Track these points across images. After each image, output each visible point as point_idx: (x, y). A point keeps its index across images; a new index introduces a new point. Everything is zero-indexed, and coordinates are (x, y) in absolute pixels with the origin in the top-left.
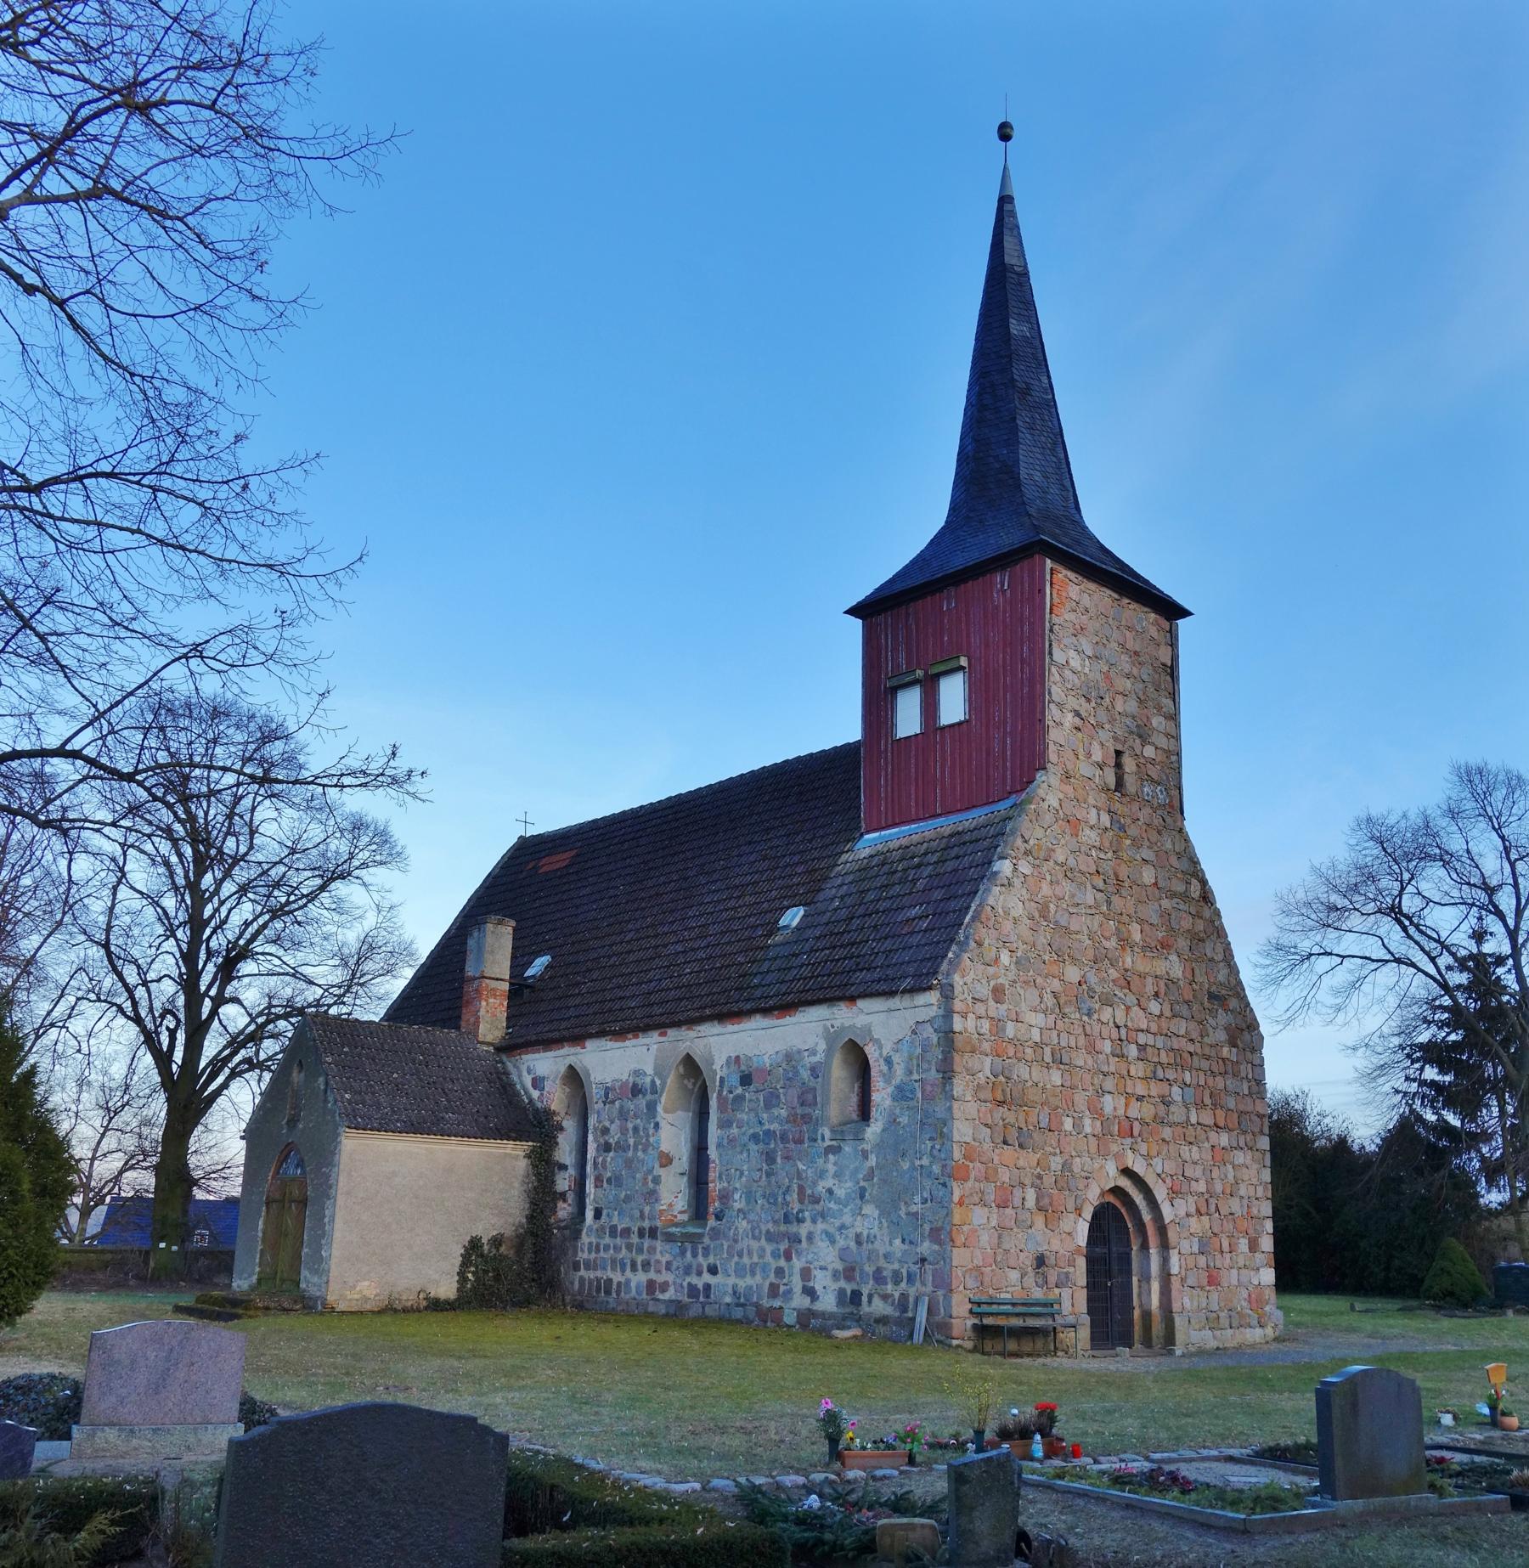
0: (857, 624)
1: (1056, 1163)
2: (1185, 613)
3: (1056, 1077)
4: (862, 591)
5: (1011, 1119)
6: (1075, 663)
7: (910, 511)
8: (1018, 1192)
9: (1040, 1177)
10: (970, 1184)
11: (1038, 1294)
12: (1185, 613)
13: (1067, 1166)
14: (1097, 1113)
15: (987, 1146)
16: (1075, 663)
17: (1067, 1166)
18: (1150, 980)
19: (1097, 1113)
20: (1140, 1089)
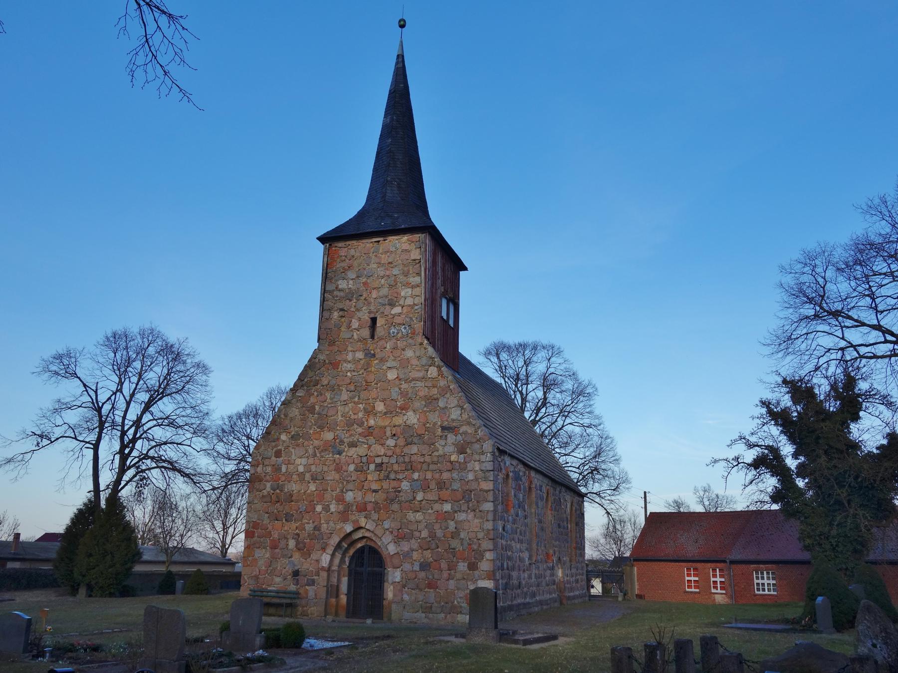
0: (320, 247)
1: (309, 527)
2: (465, 269)
3: (312, 487)
4: (319, 235)
5: (281, 508)
6: (832, 404)
7: (350, 199)
8: (283, 542)
9: (298, 535)
10: (255, 539)
11: (293, 588)
12: (465, 269)
13: (317, 528)
14: (340, 499)
15: (266, 521)
16: (832, 404)
17: (317, 528)
18: (388, 429)
19: (340, 499)
20: (375, 486)
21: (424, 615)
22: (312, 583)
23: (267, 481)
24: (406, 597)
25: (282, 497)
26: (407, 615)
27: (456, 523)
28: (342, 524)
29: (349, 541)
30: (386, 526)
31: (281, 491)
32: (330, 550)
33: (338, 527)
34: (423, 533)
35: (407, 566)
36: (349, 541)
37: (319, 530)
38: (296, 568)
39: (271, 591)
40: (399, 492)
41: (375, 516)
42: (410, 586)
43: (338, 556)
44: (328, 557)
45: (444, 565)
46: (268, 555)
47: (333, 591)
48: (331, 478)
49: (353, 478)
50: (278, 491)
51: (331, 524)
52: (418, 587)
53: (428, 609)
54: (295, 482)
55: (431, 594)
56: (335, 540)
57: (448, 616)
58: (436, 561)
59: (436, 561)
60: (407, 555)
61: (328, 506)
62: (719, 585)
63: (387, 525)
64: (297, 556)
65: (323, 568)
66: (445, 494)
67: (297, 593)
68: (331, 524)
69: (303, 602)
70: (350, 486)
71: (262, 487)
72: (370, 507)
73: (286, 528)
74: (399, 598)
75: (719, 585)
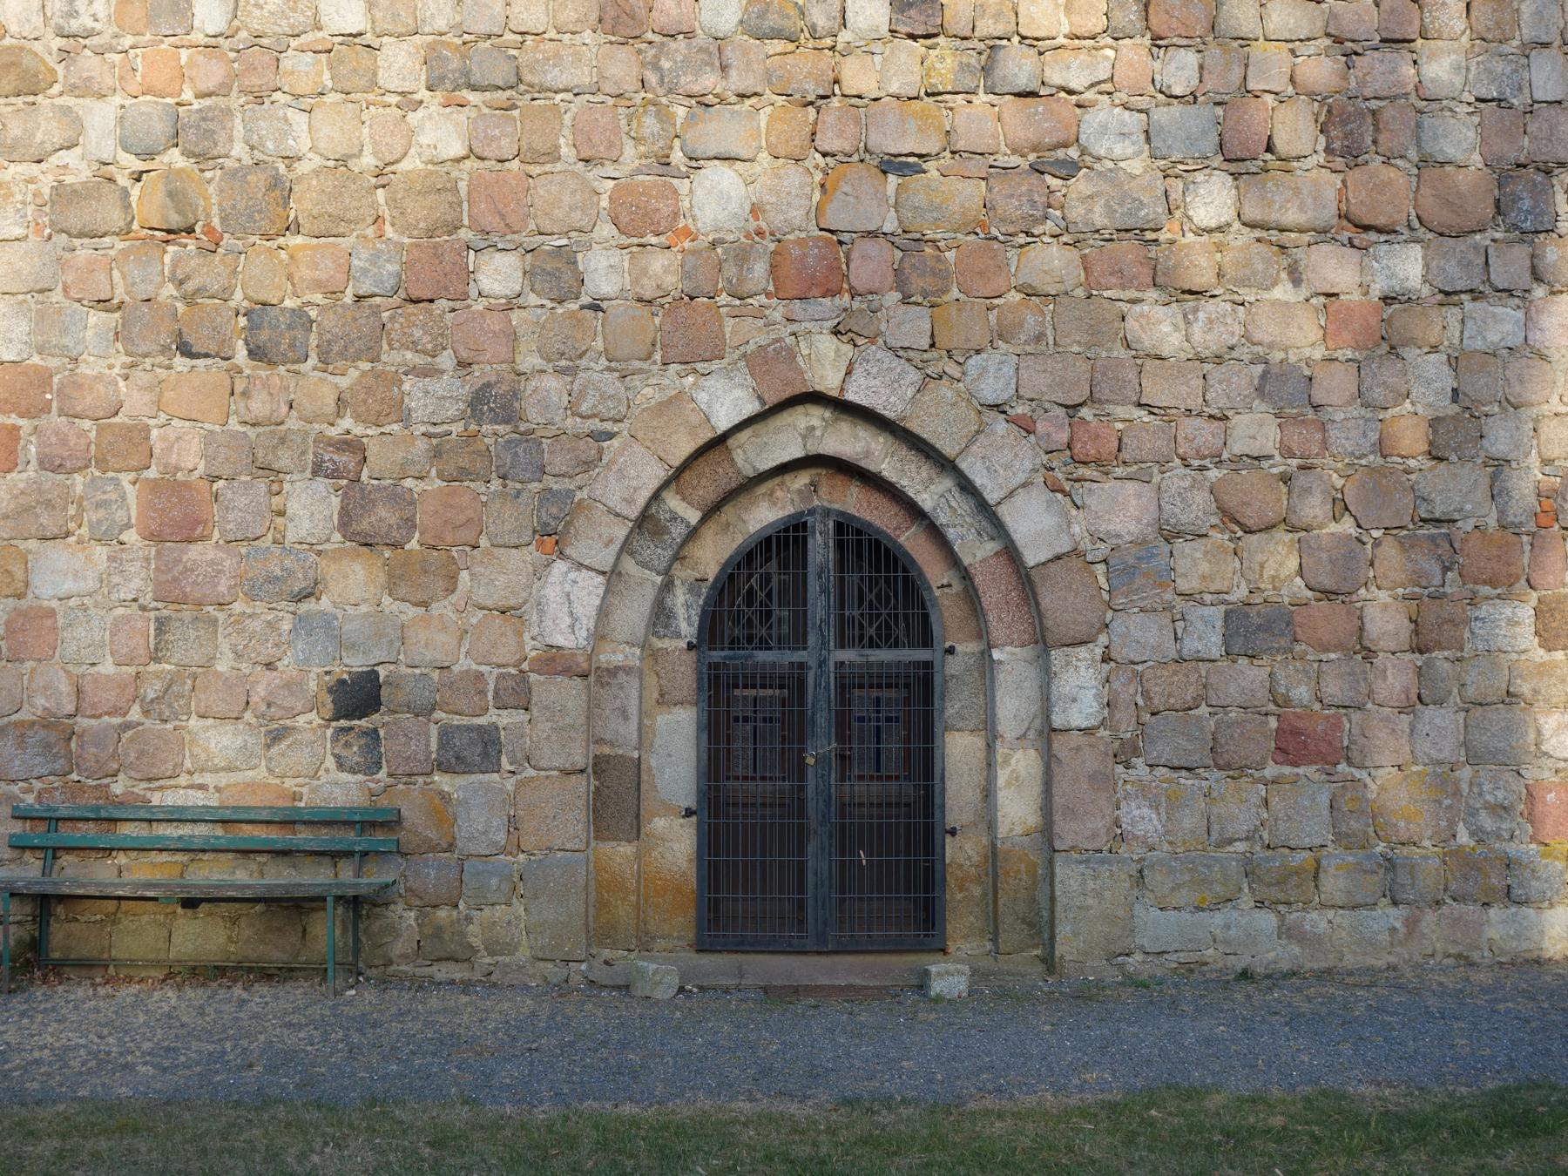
5: (208, 273)
21: (1267, 921)
22: (477, 751)
23: (85, 89)
24: (1142, 819)
25: (211, 201)
26: (1162, 928)
27: (1454, 362)
28: (674, 379)
29: (708, 484)
30: (993, 388)
31: (201, 157)
32: (599, 541)
33: (648, 394)
34: (1241, 423)
35: (1140, 634)
36: (708, 484)
37: (508, 412)
38: (357, 663)
39: (177, 816)
40: (1069, 170)
41: (913, 326)
42: (1163, 751)
43: (644, 580)
44: (589, 590)
45: (1384, 615)
46: (136, 582)
47: (614, 792)
48: (582, 76)
49: (738, 80)
50: (175, 158)
51: (595, 372)
52: (1221, 759)
53: (1279, 880)
54: (309, 101)
55: (1303, 808)
56: (633, 475)
57: (1429, 917)
58: (1328, 594)
59: (1328, 594)
60: (1133, 569)
61: (567, 257)
62: (818, 860)
63: (993, 376)
64: (354, 585)
65: (554, 662)
66: (1388, 186)
67: (376, 823)
68: (595, 372)
69: (430, 874)
70: (719, 131)
71: (47, 130)
72: (870, 264)
73: (259, 406)
74: (1100, 824)
75: (818, 860)
